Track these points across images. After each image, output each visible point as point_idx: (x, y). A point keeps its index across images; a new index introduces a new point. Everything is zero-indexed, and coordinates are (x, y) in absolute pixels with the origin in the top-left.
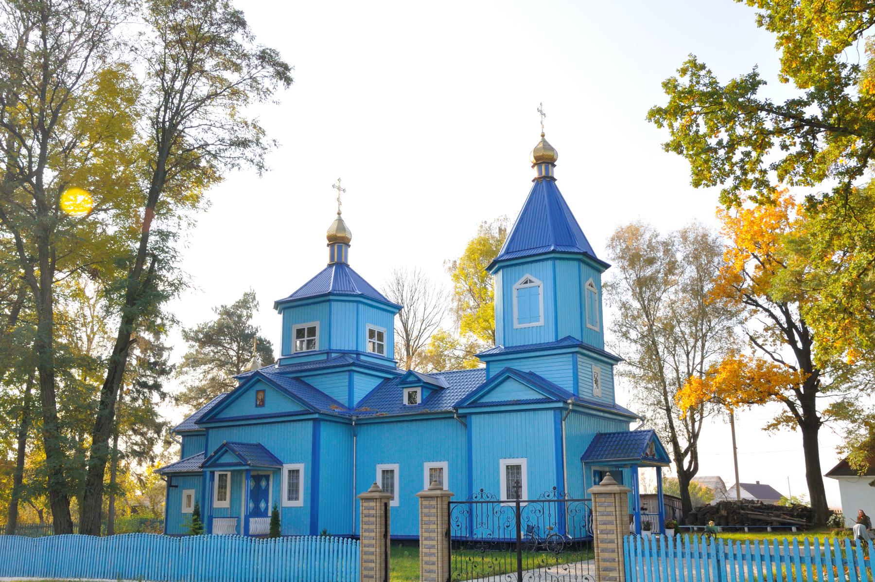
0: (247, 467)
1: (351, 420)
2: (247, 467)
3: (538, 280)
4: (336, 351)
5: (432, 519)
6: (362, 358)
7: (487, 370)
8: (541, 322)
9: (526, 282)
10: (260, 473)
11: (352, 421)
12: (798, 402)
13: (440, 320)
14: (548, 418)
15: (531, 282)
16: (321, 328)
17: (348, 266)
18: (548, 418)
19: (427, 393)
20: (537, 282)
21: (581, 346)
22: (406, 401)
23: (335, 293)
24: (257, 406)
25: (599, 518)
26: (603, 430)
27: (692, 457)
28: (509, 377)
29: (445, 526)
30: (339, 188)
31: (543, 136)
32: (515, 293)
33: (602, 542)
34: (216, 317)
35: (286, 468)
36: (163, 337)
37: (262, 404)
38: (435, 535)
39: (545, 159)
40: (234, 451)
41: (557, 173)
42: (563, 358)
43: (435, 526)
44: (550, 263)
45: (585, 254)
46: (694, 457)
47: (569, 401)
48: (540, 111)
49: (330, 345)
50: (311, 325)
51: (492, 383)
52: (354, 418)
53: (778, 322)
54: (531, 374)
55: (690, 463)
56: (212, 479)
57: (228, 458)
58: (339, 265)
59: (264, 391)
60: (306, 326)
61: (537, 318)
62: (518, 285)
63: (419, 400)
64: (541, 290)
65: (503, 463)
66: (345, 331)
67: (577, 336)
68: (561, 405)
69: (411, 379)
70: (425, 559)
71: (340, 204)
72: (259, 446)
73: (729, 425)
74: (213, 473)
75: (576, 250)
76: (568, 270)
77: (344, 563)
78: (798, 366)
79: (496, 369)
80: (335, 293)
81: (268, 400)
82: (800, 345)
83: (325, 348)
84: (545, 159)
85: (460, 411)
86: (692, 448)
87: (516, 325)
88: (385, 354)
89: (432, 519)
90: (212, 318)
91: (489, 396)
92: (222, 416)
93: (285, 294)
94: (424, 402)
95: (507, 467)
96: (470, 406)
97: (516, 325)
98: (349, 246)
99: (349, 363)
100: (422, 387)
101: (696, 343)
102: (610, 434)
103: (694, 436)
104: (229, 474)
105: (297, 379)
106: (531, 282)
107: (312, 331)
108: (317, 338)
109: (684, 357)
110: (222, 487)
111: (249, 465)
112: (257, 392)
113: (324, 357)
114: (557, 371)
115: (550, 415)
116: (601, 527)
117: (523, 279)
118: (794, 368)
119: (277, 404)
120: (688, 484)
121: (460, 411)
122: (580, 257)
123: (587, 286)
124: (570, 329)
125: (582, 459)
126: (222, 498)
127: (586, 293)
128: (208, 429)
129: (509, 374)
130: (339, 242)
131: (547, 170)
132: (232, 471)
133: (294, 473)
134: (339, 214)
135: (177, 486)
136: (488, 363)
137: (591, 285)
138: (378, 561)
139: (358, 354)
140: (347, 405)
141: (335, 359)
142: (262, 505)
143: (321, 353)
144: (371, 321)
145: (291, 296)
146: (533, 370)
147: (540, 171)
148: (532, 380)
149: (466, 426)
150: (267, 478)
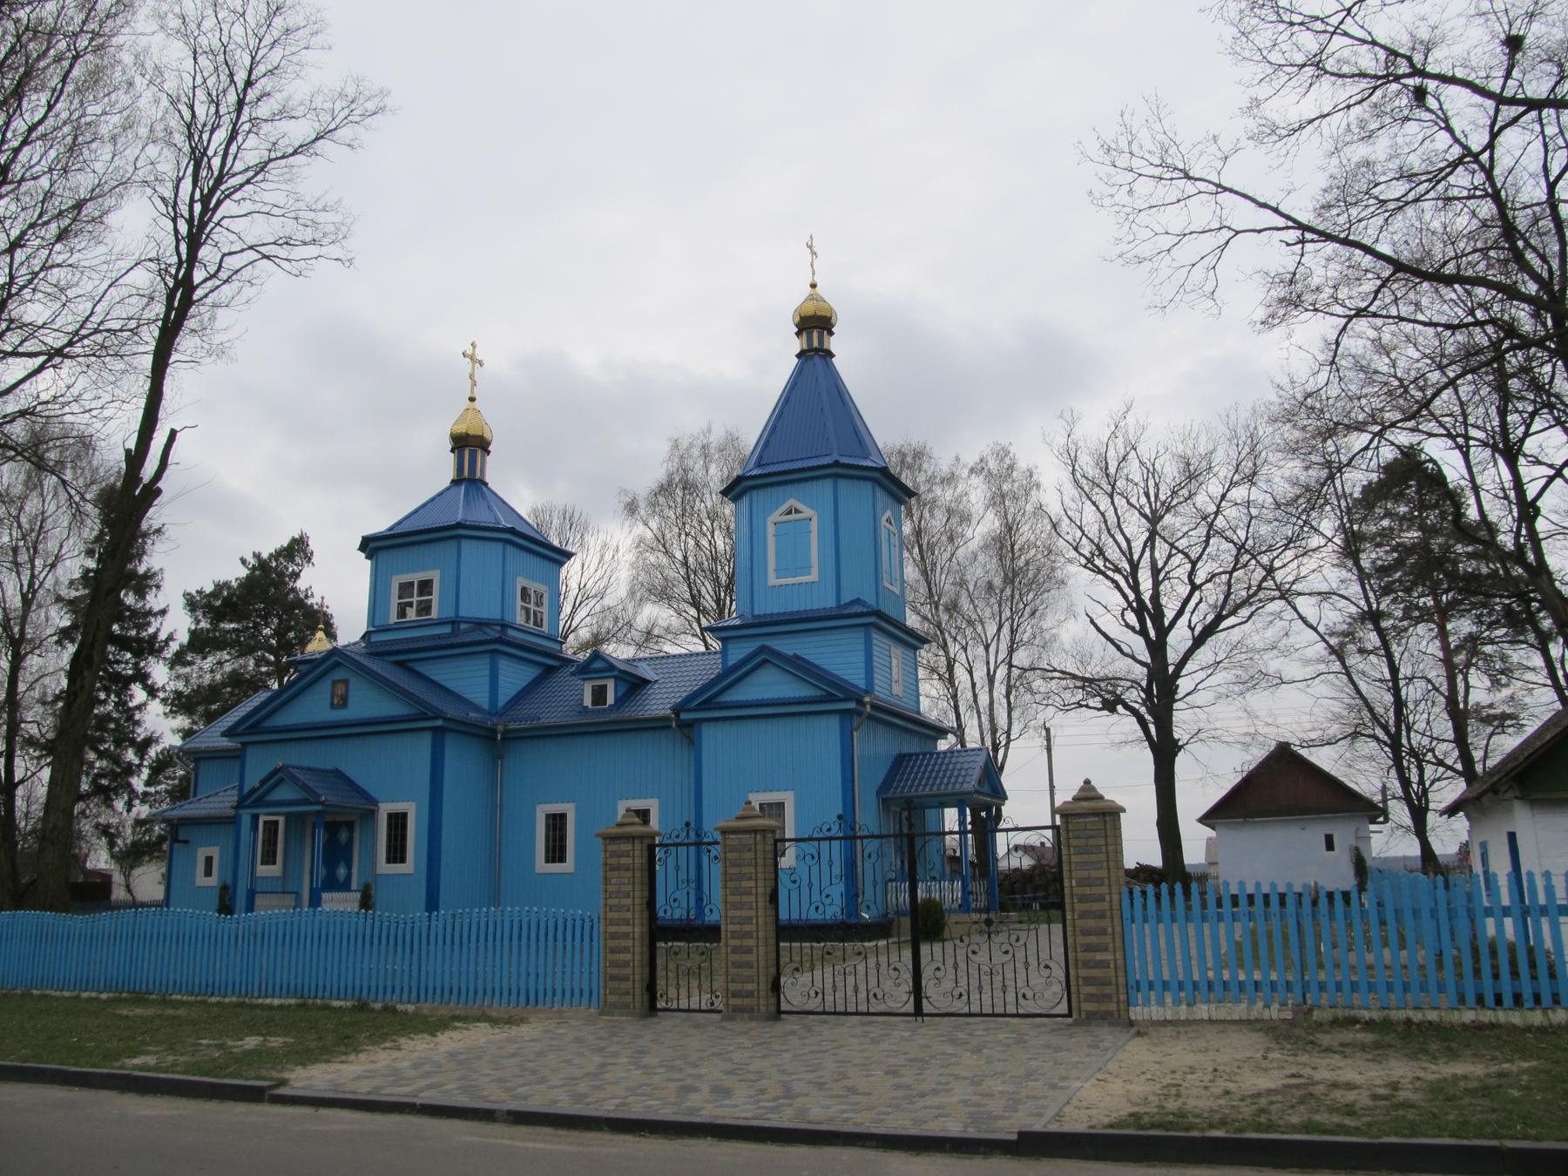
0: (319, 808)
1: (494, 731)
2: (319, 808)
3: (807, 510)
4: (468, 621)
5: (746, 870)
6: (510, 632)
7: (724, 652)
8: (814, 576)
9: (790, 513)
10: (338, 819)
11: (496, 737)
13: (614, 584)
15: (797, 511)
16: (441, 582)
17: (486, 484)
19: (623, 689)
20: (808, 512)
21: (879, 614)
22: (588, 702)
23: (461, 533)
24: (333, 706)
25: (1074, 859)
26: (906, 750)
28: (765, 662)
29: (771, 883)
30: (472, 358)
31: (813, 286)
32: (771, 530)
33: (1081, 901)
34: (243, 573)
35: (385, 809)
36: (150, 597)
37: (344, 702)
38: (752, 898)
40: (295, 780)
41: (834, 344)
42: (846, 636)
43: (751, 884)
48: (810, 247)
50: (424, 576)
51: (733, 675)
52: (500, 728)
54: (796, 656)
56: (255, 828)
57: (284, 793)
58: (469, 480)
59: (346, 682)
60: (416, 577)
61: (807, 569)
62: (776, 516)
63: (610, 699)
64: (814, 525)
66: (477, 586)
67: (870, 599)
68: (852, 705)
69: (598, 665)
70: (733, 942)
71: (474, 384)
72: (338, 773)
74: (255, 818)
75: (870, 464)
76: (858, 497)
77: (568, 962)
79: (739, 652)
80: (461, 533)
82: (1152, 634)
83: (450, 614)
84: (815, 323)
85: (683, 716)
87: (773, 580)
88: (545, 628)
89: (746, 870)
90: (235, 573)
91: (733, 690)
92: (269, 723)
93: (380, 523)
94: (621, 701)
96: (699, 708)
97: (773, 580)
98: (489, 453)
99: (491, 639)
100: (616, 678)
101: (999, 630)
102: (911, 755)
104: (281, 819)
106: (797, 511)
107: (425, 586)
108: (435, 598)
109: (981, 650)
110: (270, 842)
111: (322, 803)
113: (447, 629)
114: (839, 656)
115: (833, 723)
116: (1077, 874)
117: (785, 507)
119: (366, 703)
121: (683, 716)
122: (877, 475)
123: (884, 522)
124: (857, 588)
125: (878, 793)
126: (269, 858)
127: (884, 533)
128: (244, 745)
129: (764, 659)
131: (821, 341)
132: (288, 816)
135: (186, 842)
136: (723, 640)
137: (889, 521)
138: (637, 950)
139: (505, 626)
140: (486, 706)
141: (466, 632)
142: (342, 872)
143: (441, 623)
144: (525, 574)
145: (391, 529)
146: (799, 653)
147: (810, 340)
148: (799, 667)
149: (691, 742)
150: (350, 826)
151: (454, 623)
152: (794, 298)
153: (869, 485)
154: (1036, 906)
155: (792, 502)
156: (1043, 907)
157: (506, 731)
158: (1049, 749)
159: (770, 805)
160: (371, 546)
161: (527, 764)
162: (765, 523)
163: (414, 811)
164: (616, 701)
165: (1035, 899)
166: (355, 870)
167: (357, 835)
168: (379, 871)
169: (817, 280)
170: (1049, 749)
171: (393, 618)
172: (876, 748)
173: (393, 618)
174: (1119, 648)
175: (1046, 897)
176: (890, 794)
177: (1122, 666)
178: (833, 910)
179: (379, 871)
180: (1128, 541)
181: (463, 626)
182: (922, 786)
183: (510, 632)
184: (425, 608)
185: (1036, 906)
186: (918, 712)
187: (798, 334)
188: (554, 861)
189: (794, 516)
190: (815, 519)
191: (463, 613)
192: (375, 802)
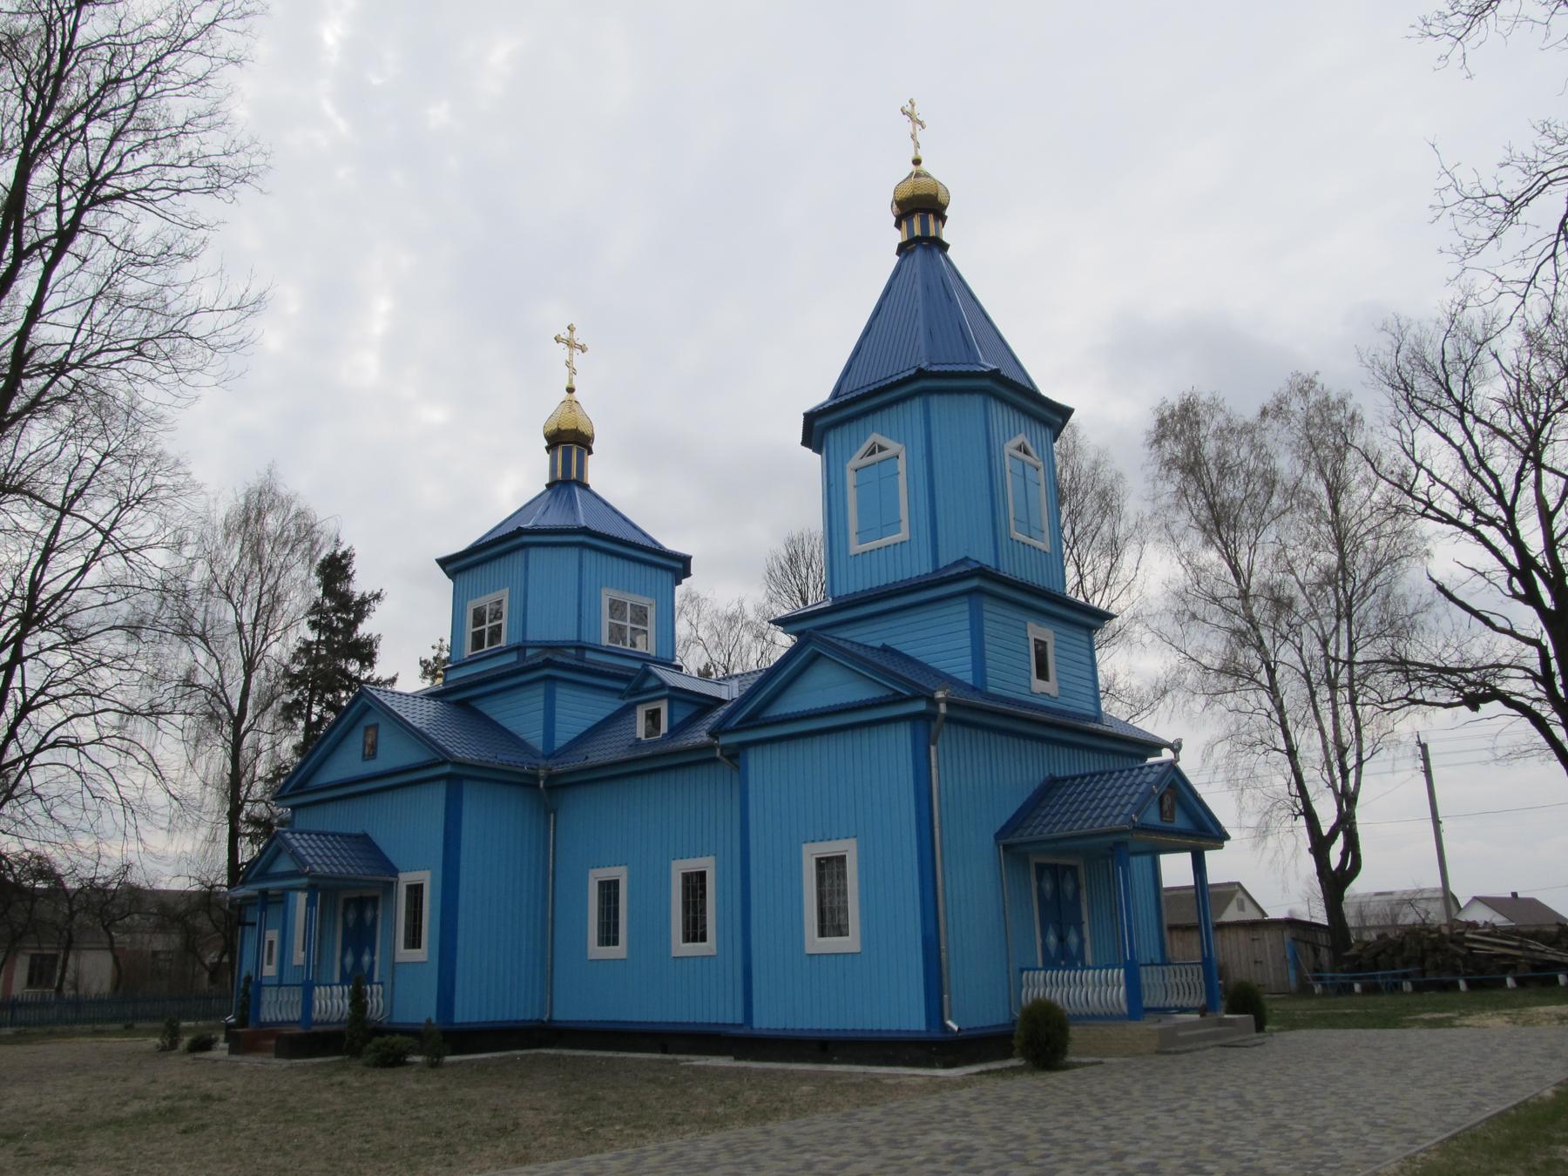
1: (536, 778)
6: (589, 655)
8: (903, 535)
9: (873, 452)
10: (367, 894)
11: (549, 786)
12: (1555, 716)
14: (899, 741)
15: (882, 449)
17: (586, 487)
18: (899, 741)
20: (893, 447)
23: (565, 547)
26: (1060, 772)
27: (1346, 843)
30: (570, 344)
32: (851, 478)
35: (405, 879)
37: (371, 753)
39: (921, 209)
44: (573, 553)
45: (995, 375)
46: (1352, 845)
47: (940, 695)
49: (524, 633)
52: (542, 773)
53: (1503, 560)
55: (1344, 855)
58: (566, 484)
59: (376, 726)
61: (894, 526)
62: (856, 461)
63: (664, 728)
64: (901, 465)
65: (810, 854)
66: (597, 608)
67: (986, 559)
68: (921, 706)
73: (1422, 777)
78: (1546, 640)
80: (565, 547)
81: (382, 750)
83: (517, 640)
84: (921, 209)
86: (1346, 822)
87: (855, 548)
94: (675, 730)
95: (819, 860)
98: (590, 452)
100: (671, 699)
103: (1347, 799)
105: (463, 705)
106: (882, 449)
112: (367, 728)
114: (940, 642)
117: (865, 447)
118: (1536, 643)
120: (1341, 898)
122: (986, 383)
124: (966, 541)
125: (998, 836)
130: (569, 442)
131: (925, 226)
133: (415, 891)
134: (570, 390)
137: (1022, 448)
146: (888, 642)
147: (910, 229)
150: (374, 900)
151: (519, 649)
152: (891, 177)
153: (977, 400)
154: (1407, 986)
155: (876, 438)
156: (1418, 988)
157: (551, 777)
158: (1427, 772)
159: (829, 859)
160: (453, 565)
161: (587, 817)
162: (843, 468)
163: (426, 877)
164: (671, 729)
165: (1406, 976)
166: (377, 958)
167: (380, 913)
168: (398, 959)
169: (921, 154)
170: (1427, 772)
171: (468, 651)
172: (1012, 774)
173: (468, 651)
174: (1487, 621)
175: (1423, 973)
176: (1014, 840)
177: (1505, 648)
178: (910, 1017)
179: (398, 959)
180: (1494, 477)
181: (529, 652)
182: (1095, 819)
183: (589, 655)
184: (496, 633)
185: (1407, 986)
186: (1098, 717)
187: (898, 225)
188: (695, 940)
189: (879, 456)
190: (902, 456)
191: (530, 637)
192: (394, 872)
